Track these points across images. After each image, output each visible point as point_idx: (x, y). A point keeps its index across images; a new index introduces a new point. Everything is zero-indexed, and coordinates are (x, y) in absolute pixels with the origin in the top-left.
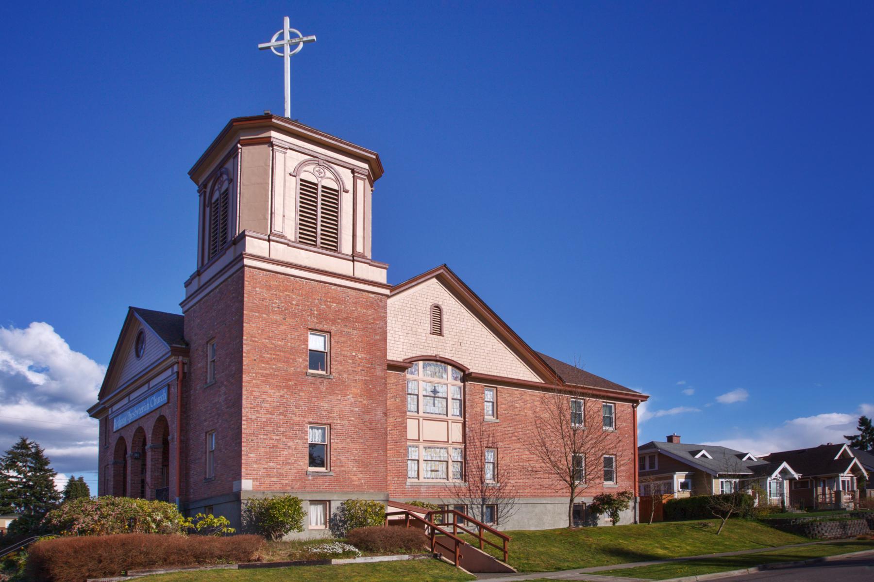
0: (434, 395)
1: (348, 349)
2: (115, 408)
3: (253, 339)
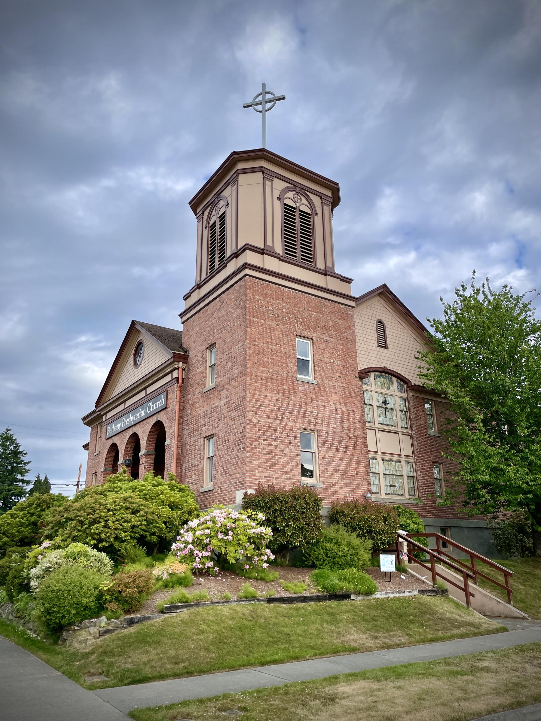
0: (384, 406)
1: (327, 356)
2: (109, 415)
3: (254, 343)
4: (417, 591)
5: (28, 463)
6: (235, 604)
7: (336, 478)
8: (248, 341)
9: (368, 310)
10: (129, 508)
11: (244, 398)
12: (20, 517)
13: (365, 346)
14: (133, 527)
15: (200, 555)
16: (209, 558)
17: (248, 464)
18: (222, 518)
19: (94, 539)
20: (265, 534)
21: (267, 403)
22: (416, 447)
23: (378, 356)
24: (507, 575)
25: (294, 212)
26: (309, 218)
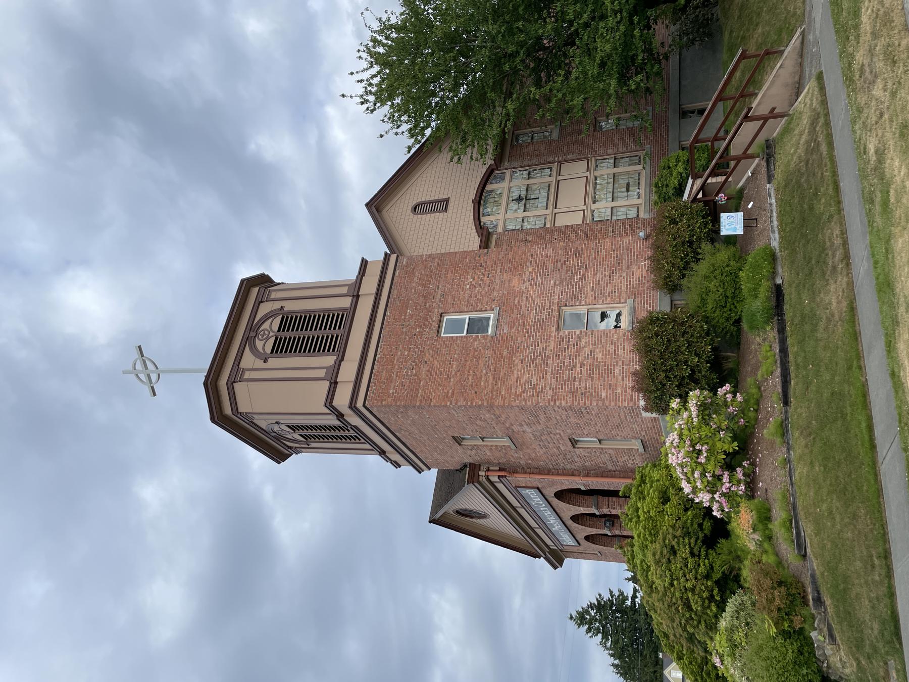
3: (450, 394)
4: (768, 185)
5: (611, 592)
6: (792, 453)
7: (621, 279)
8: (449, 403)
9: (401, 227)
10: (669, 559)
11: (522, 408)
12: (681, 649)
13: (447, 230)
14: (692, 554)
15: (728, 485)
16: (732, 474)
17: (607, 403)
18: (679, 456)
19: (709, 607)
20: (698, 401)
21: (526, 376)
22: (576, 156)
23: (459, 212)
24: (744, 56)
25: (281, 339)
26: (287, 318)
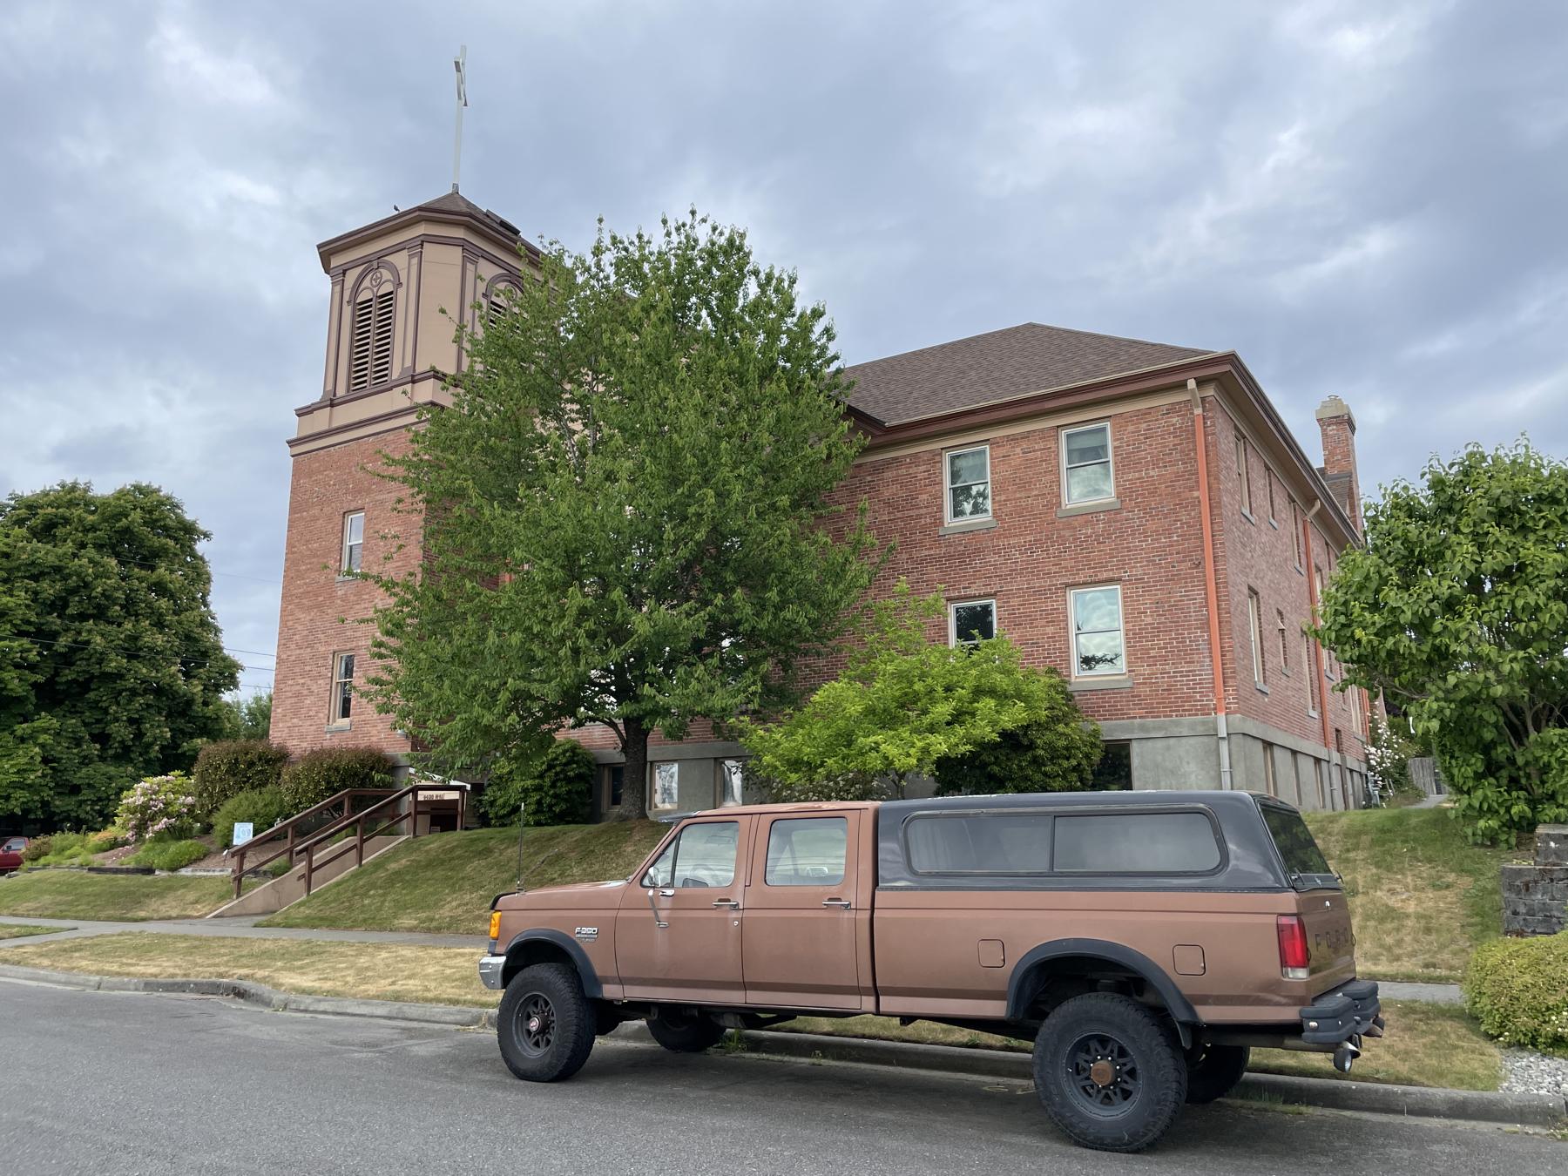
21: (300, 628)
